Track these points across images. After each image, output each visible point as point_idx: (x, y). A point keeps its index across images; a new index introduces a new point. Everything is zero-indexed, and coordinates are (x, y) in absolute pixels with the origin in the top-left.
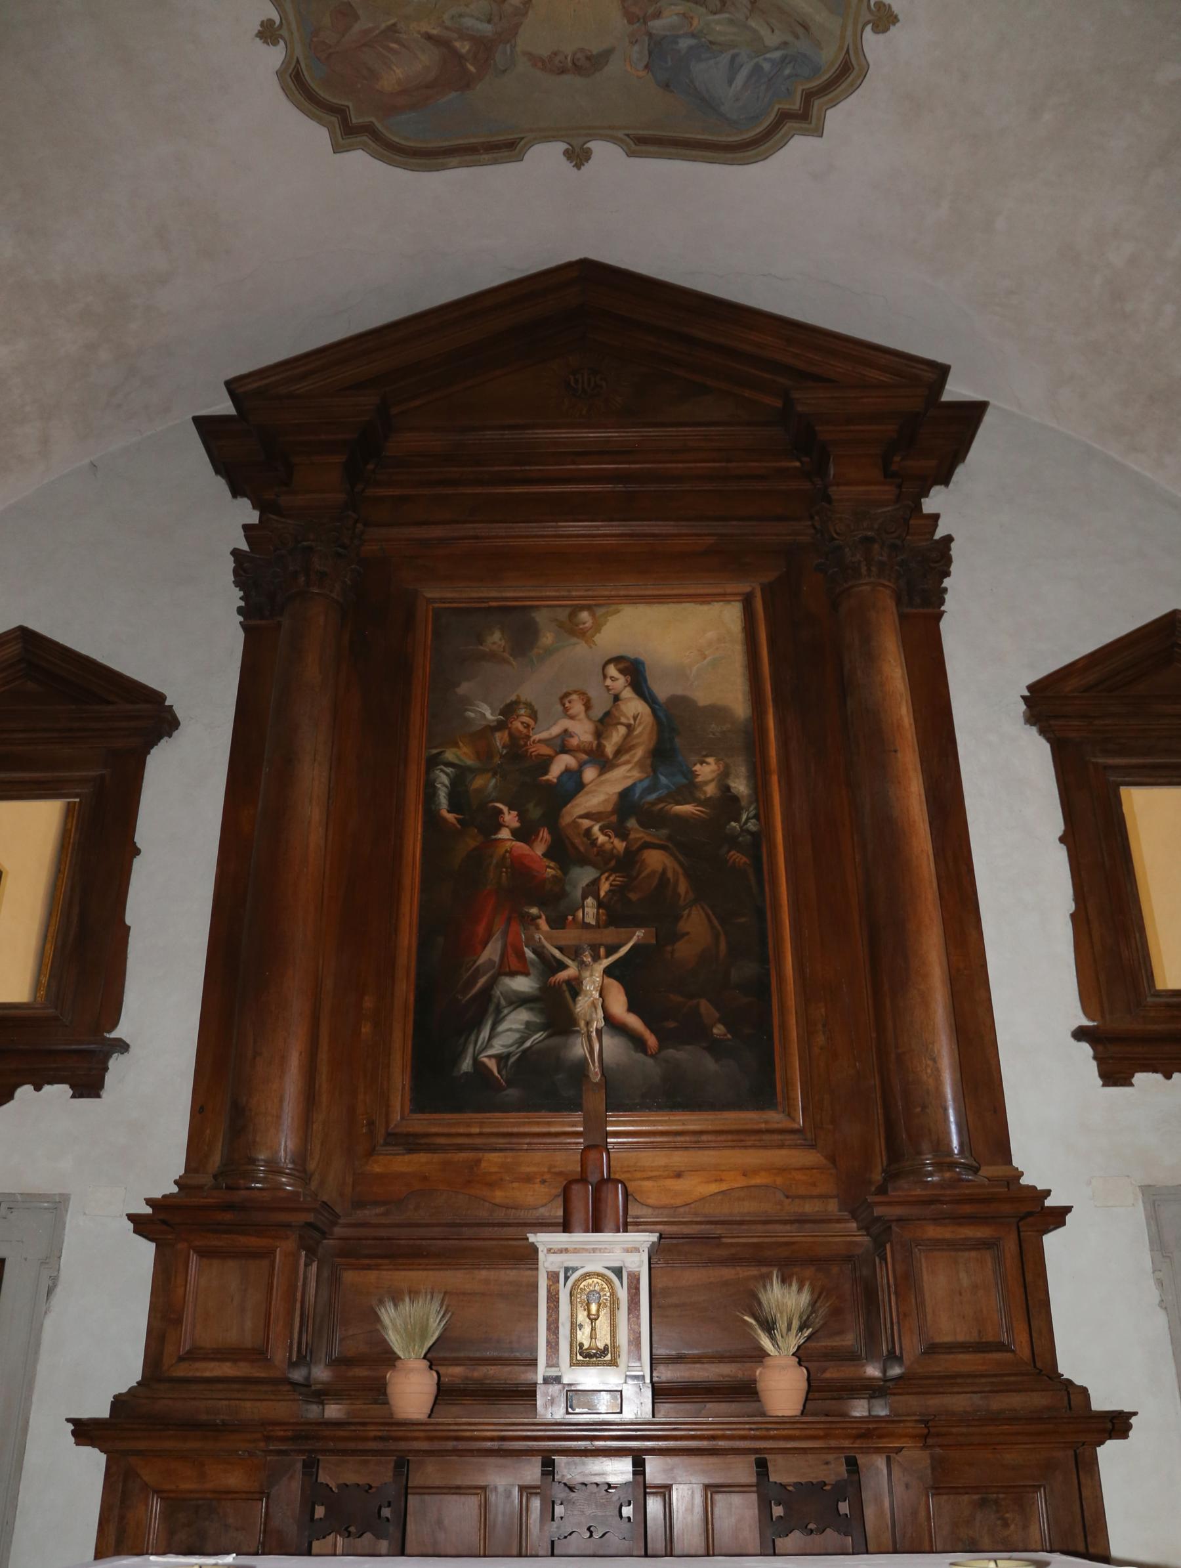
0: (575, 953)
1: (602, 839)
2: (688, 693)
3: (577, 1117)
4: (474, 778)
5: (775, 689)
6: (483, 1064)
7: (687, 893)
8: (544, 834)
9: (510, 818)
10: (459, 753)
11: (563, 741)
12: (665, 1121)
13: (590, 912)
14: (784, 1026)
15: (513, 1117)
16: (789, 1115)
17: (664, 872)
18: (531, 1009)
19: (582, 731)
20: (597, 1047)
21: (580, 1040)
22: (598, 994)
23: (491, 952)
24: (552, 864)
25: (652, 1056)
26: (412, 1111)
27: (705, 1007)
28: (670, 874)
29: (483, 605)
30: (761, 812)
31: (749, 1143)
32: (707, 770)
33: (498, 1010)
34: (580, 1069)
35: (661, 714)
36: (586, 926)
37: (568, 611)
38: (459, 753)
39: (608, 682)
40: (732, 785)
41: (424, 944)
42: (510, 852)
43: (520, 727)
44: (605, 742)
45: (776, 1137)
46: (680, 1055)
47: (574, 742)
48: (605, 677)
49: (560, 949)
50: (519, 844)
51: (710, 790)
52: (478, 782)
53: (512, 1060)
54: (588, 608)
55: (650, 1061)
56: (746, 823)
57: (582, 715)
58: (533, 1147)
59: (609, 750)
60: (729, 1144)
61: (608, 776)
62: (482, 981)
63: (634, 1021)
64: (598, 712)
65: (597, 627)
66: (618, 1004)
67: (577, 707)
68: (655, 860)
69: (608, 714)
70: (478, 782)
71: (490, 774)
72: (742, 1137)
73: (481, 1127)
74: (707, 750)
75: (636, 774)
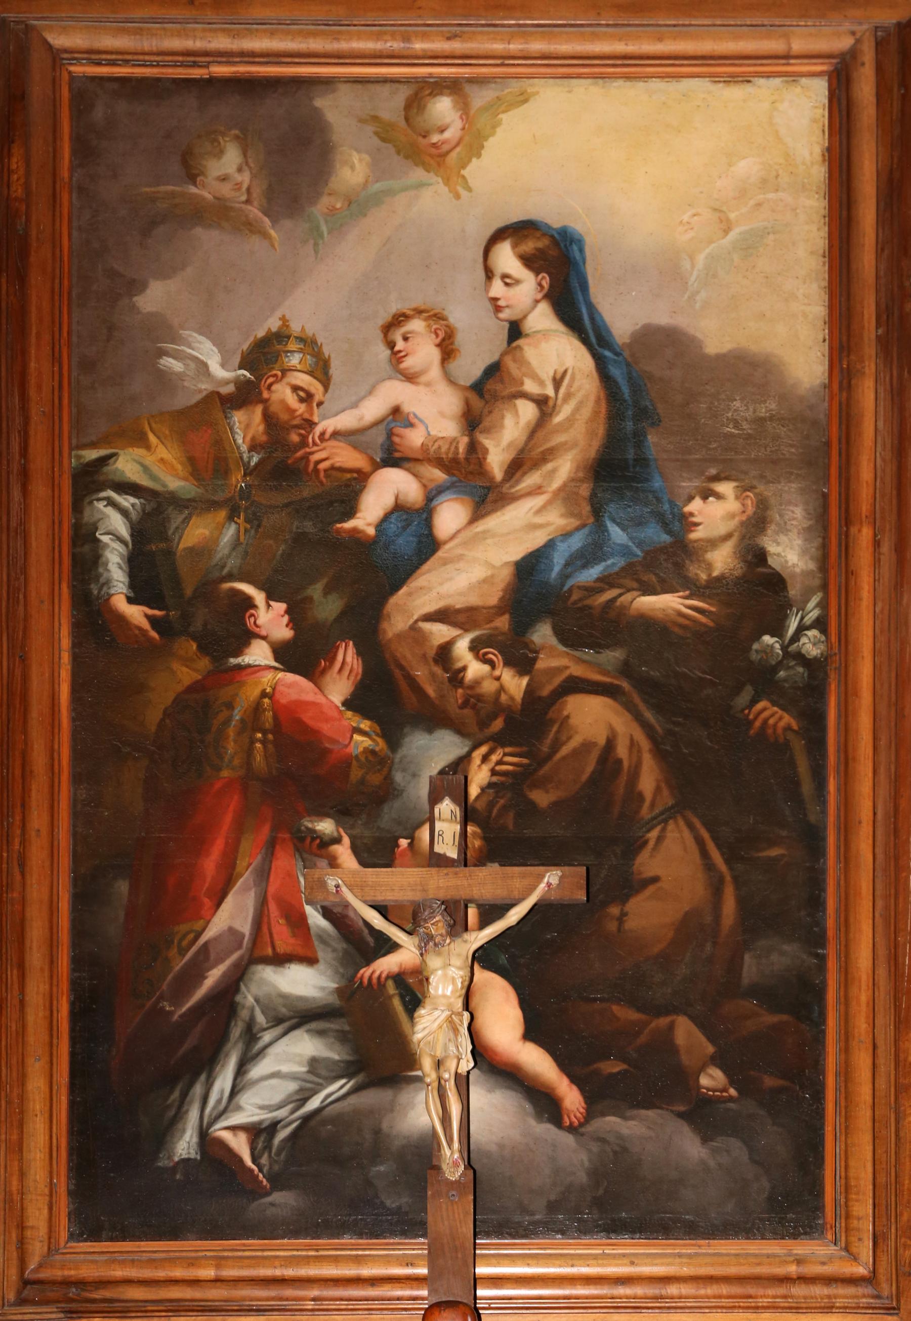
0: (411, 917)
1: (475, 669)
2: (681, 321)
3: (417, 1247)
4: (187, 520)
5: (885, 315)
6: (221, 1143)
7: (658, 790)
8: (348, 655)
9: (271, 618)
10: (149, 460)
11: (390, 434)
12: (595, 1257)
13: (446, 830)
14: (846, 1073)
15: (285, 1247)
16: (847, 1249)
17: (610, 744)
18: (321, 1033)
19: (435, 415)
20: (455, 1109)
21: (421, 1096)
22: (462, 1007)
23: (233, 914)
24: (365, 725)
25: (572, 1129)
26: (72, 1237)
27: (686, 1032)
28: (622, 751)
29: (196, 73)
30: (833, 612)
31: (764, 1302)
32: (715, 515)
33: (251, 1035)
34: (421, 1156)
35: (616, 372)
36: (438, 861)
37: (403, 93)
38: (149, 460)
39: (497, 288)
40: (772, 548)
41: (87, 894)
42: (271, 697)
43: (291, 399)
44: (487, 441)
45: (819, 1290)
46: (630, 1127)
47: (415, 438)
48: (489, 274)
49: (382, 910)
50: (291, 677)
51: (722, 560)
52: (196, 532)
53: (283, 1134)
54: (453, 87)
55: (568, 1139)
56: (796, 637)
57: (435, 372)
58: (326, 1305)
59: (496, 459)
60: (724, 1302)
61: (495, 522)
62: (214, 976)
63: (536, 1061)
64: (470, 366)
65: (473, 142)
66: (503, 1019)
67: (423, 352)
68: (592, 718)
69: (494, 370)
70: (196, 532)
71: (223, 514)
72: (751, 1290)
73: (218, 1267)
74: (722, 462)
75: (556, 520)
